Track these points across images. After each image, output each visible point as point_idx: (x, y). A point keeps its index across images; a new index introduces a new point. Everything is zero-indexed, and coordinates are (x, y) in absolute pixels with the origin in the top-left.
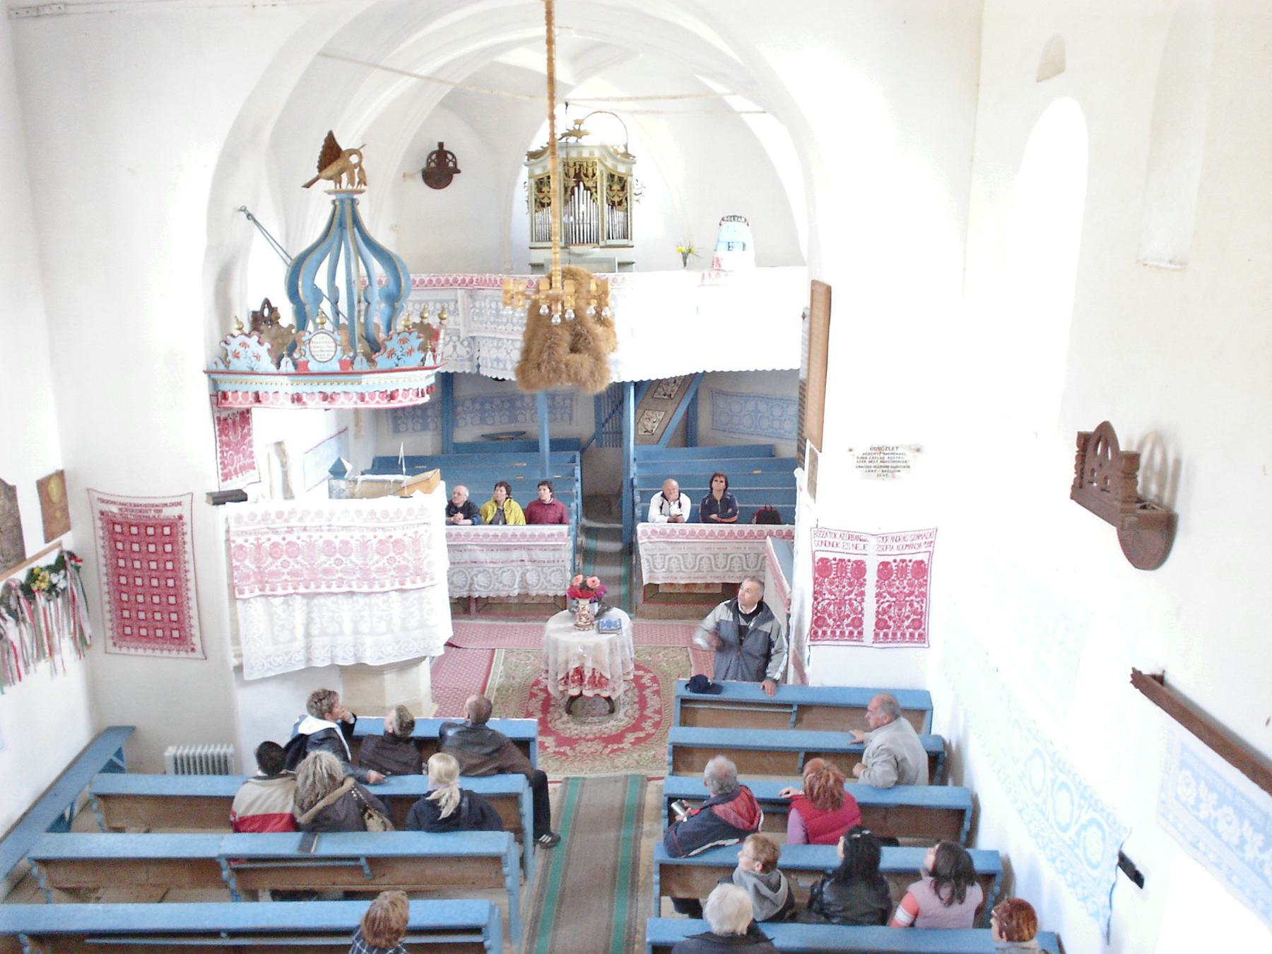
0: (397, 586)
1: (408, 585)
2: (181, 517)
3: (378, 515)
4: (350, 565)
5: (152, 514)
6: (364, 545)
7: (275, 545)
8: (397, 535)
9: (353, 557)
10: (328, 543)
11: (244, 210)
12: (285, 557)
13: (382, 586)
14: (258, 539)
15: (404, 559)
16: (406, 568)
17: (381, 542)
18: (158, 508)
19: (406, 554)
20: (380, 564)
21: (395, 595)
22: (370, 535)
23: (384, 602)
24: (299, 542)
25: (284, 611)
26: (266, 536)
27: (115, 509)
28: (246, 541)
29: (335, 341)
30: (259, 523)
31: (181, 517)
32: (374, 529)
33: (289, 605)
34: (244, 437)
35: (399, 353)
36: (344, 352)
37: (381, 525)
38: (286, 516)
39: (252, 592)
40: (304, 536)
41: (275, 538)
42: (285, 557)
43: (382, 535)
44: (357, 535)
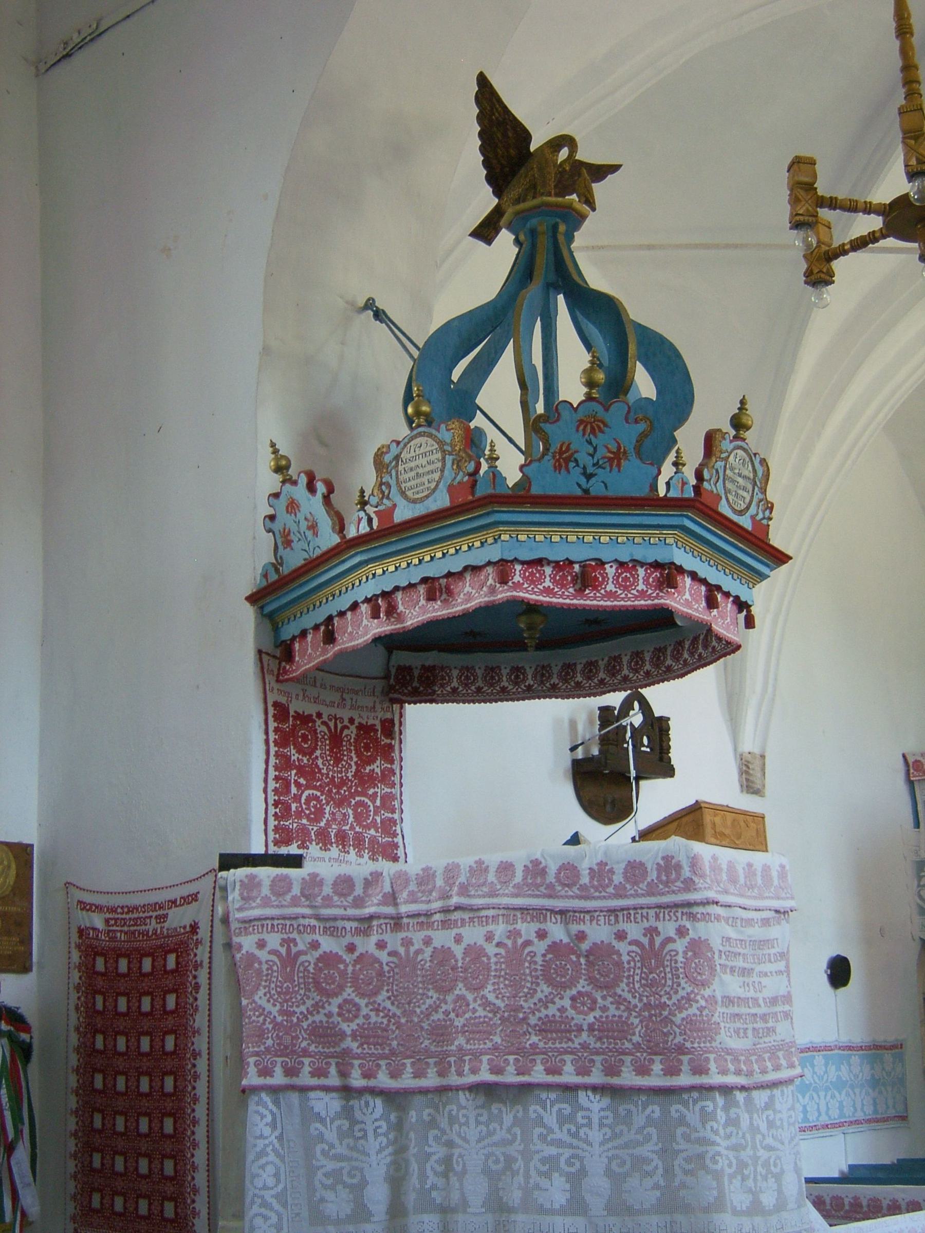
0: (596, 1077)
1: (628, 1078)
2: (194, 928)
3: (551, 878)
4: (481, 1012)
5: (152, 925)
6: (516, 954)
7: (329, 959)
8: (599, 932)
9: (488, 992)
10: (443, 956)
11: (370, 304)
12: (349, 992)
13: (556, 1071)
14: (287, 942)
15: (619, 1001)
16: (621, 1030)
17: (554, 948)
18: (160, 909)
19: (622, 989)
20: (552, 1010)
21: (595, 1104)
22: (527, 929)
23: (562, 1120)
24: (383, 956)
25: (342, 1135)
26: (309, 938)
27: (98, 921)
28: (261, 944)
29: (441, 443)
30: (295, 902)
31: (194, 928)
32: (539, 914)
33: (354, 1122)
34: (365, 781)
35: (584, 458)
36: (458, 463)
37: (559, 904)
38: (359, 890)
39: (265, 1072)
40: (394, 941)
41: (328, 944)
42: (349, 992)
43: (558, 932)
44: (500, 929)
